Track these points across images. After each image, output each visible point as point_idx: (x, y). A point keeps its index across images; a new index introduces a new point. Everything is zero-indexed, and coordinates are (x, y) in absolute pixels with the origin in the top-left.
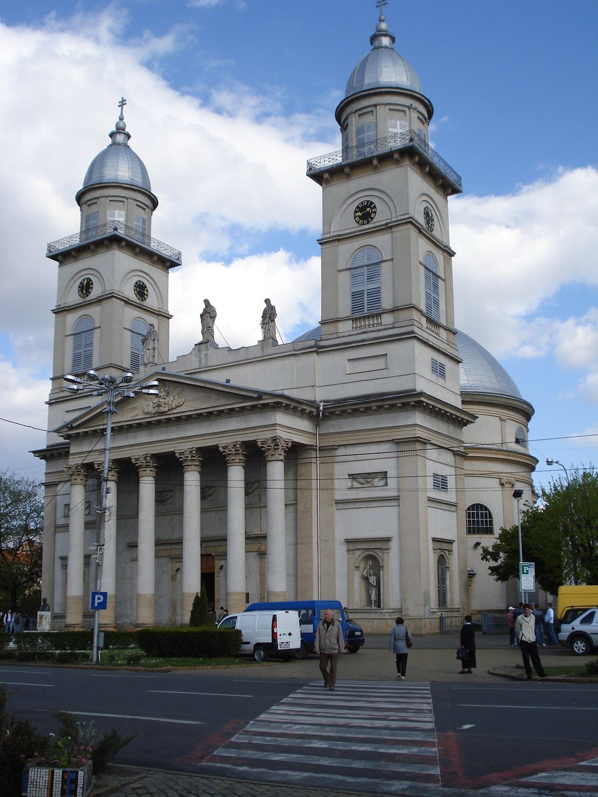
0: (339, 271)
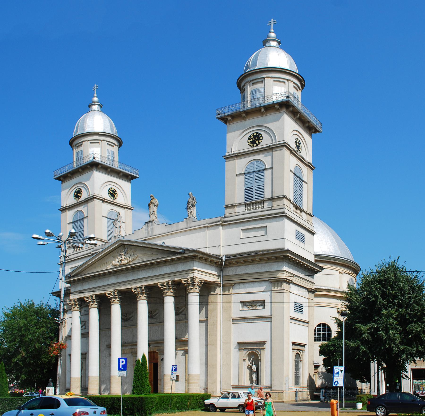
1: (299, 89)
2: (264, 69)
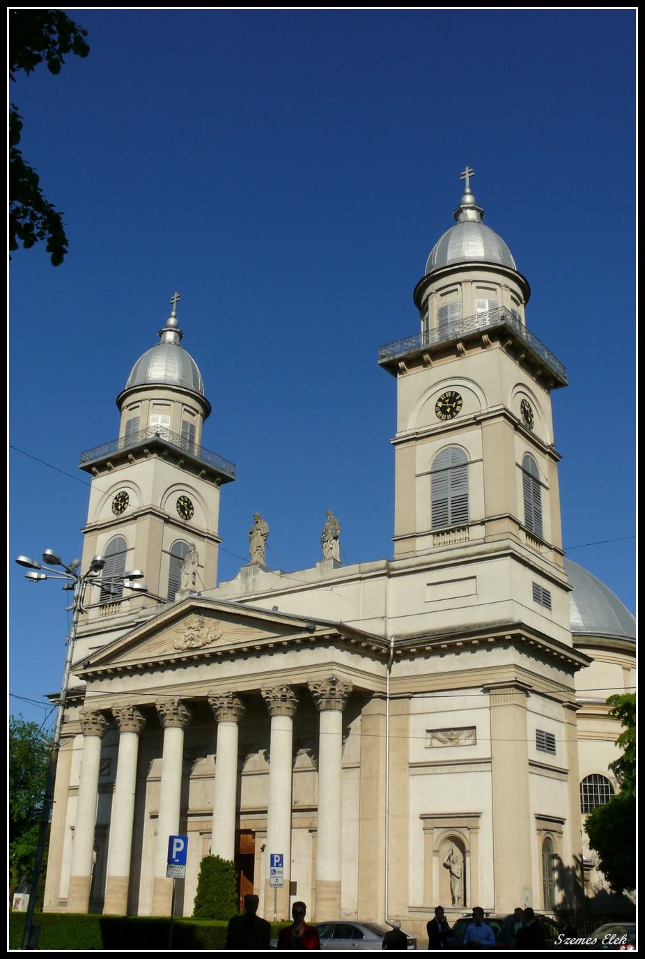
0: (417, 476)
1: (521, 301)
2: (459, 266)
